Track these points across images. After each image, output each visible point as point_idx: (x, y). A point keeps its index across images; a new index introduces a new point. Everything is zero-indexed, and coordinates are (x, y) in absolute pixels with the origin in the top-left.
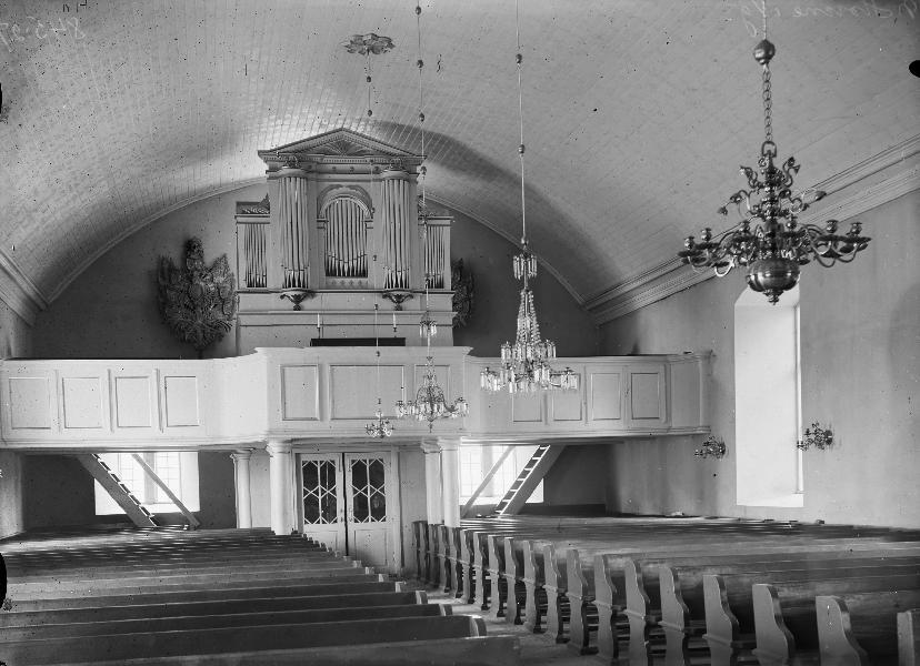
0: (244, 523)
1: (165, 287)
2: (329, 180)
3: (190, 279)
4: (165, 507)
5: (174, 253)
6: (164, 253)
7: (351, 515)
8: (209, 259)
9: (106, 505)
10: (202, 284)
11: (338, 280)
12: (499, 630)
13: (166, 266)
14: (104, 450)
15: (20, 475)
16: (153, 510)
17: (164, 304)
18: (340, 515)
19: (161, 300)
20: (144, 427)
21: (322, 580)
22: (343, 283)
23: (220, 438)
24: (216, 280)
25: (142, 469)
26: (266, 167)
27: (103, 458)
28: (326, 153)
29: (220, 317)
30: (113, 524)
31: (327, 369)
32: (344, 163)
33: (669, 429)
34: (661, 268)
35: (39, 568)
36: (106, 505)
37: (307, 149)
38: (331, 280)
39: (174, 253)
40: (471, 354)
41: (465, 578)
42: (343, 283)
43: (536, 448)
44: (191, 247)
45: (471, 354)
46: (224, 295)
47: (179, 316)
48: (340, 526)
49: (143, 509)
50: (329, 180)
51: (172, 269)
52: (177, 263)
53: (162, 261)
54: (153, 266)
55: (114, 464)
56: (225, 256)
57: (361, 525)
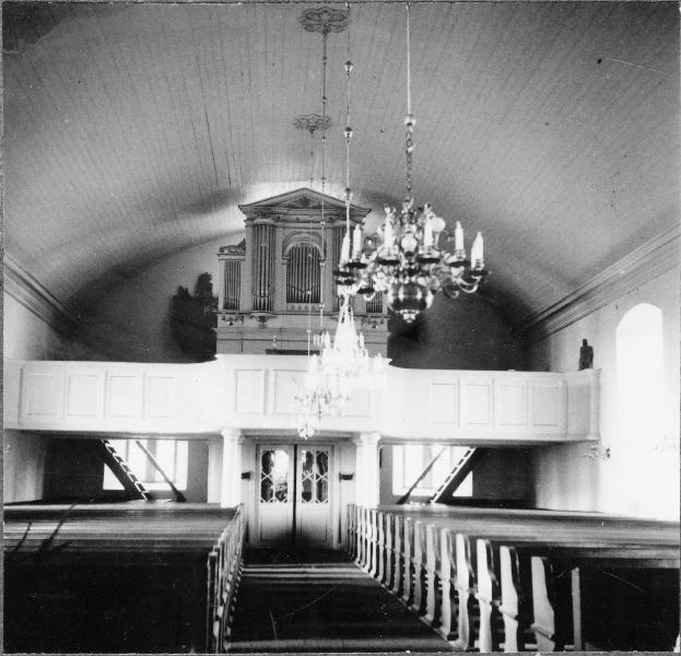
0: (211, 499)
2: (291, 228)
4: (161, 486)
5: (191, 288)
7: (299, 497)
9: (111, 482)
11: (296, 305)
14: (117, 436)
16: (148, 488)
18: (289, 496)
20: (162, 421)
21: (129, 535)
22: (300, 308)
25: (145, 456)
26: (245, 217)
27: (112, 444)
28: (290, 207)
30: (114, 497)
31: (272, 373)
32: (302, 214)
33: (566, 434)
34: (567, 306)
36: (111, 482)
37: (273, 205)
38: (290, 305)
40: (390, 364)
41: (397, 565)
42: (300, 308)
43: (468, 448)
45: (390, 364)
48: (290, 505)
49: (140, 486)
50: (291, 228)
54: (173, 292)
55: (118, 447)
57: (266, 505)
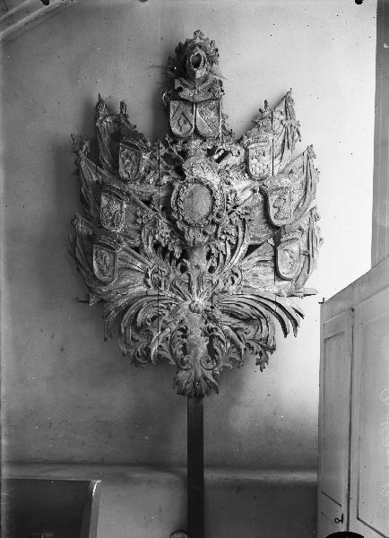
1: (100, 187)
3: (177, 165)
5: (130, 87)
6: (101, 89)
8: (237, 107)
10: (214, 179)
12: (80, 218)
13: (106, 123)
15: (138, 475)
17: (92, 239)
19: (81, 227)
23: (282, 261)
24: (256, 167)
29: (268, 287)
35: (189, 489)
39: (130, 87)
44: (184, 67)
46: (283, 214)
47: (134, 281)
51: (122, 133)
52: (141, 119)
53: (94, 111)
56: (286, 99)
